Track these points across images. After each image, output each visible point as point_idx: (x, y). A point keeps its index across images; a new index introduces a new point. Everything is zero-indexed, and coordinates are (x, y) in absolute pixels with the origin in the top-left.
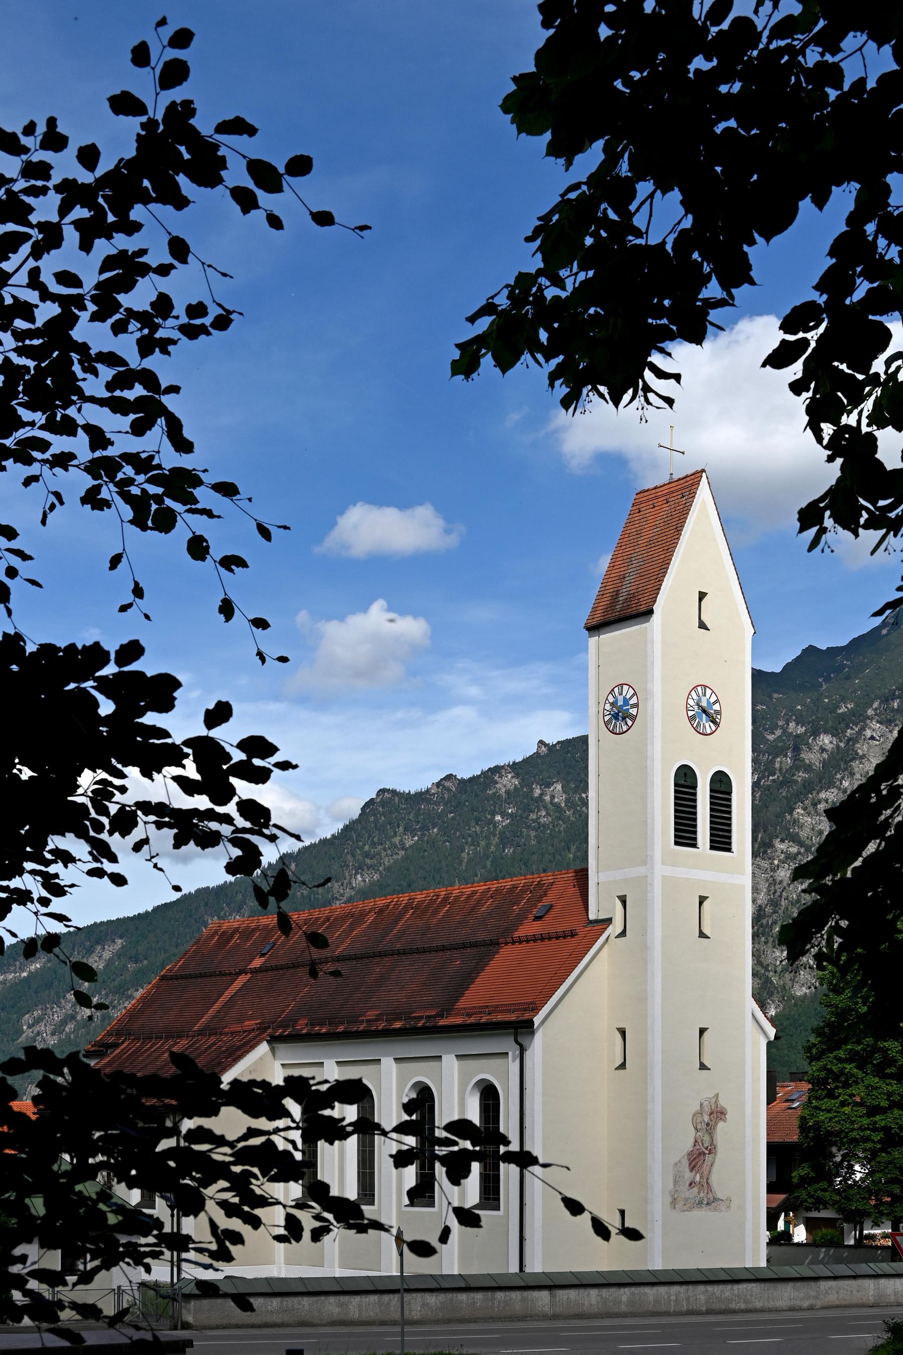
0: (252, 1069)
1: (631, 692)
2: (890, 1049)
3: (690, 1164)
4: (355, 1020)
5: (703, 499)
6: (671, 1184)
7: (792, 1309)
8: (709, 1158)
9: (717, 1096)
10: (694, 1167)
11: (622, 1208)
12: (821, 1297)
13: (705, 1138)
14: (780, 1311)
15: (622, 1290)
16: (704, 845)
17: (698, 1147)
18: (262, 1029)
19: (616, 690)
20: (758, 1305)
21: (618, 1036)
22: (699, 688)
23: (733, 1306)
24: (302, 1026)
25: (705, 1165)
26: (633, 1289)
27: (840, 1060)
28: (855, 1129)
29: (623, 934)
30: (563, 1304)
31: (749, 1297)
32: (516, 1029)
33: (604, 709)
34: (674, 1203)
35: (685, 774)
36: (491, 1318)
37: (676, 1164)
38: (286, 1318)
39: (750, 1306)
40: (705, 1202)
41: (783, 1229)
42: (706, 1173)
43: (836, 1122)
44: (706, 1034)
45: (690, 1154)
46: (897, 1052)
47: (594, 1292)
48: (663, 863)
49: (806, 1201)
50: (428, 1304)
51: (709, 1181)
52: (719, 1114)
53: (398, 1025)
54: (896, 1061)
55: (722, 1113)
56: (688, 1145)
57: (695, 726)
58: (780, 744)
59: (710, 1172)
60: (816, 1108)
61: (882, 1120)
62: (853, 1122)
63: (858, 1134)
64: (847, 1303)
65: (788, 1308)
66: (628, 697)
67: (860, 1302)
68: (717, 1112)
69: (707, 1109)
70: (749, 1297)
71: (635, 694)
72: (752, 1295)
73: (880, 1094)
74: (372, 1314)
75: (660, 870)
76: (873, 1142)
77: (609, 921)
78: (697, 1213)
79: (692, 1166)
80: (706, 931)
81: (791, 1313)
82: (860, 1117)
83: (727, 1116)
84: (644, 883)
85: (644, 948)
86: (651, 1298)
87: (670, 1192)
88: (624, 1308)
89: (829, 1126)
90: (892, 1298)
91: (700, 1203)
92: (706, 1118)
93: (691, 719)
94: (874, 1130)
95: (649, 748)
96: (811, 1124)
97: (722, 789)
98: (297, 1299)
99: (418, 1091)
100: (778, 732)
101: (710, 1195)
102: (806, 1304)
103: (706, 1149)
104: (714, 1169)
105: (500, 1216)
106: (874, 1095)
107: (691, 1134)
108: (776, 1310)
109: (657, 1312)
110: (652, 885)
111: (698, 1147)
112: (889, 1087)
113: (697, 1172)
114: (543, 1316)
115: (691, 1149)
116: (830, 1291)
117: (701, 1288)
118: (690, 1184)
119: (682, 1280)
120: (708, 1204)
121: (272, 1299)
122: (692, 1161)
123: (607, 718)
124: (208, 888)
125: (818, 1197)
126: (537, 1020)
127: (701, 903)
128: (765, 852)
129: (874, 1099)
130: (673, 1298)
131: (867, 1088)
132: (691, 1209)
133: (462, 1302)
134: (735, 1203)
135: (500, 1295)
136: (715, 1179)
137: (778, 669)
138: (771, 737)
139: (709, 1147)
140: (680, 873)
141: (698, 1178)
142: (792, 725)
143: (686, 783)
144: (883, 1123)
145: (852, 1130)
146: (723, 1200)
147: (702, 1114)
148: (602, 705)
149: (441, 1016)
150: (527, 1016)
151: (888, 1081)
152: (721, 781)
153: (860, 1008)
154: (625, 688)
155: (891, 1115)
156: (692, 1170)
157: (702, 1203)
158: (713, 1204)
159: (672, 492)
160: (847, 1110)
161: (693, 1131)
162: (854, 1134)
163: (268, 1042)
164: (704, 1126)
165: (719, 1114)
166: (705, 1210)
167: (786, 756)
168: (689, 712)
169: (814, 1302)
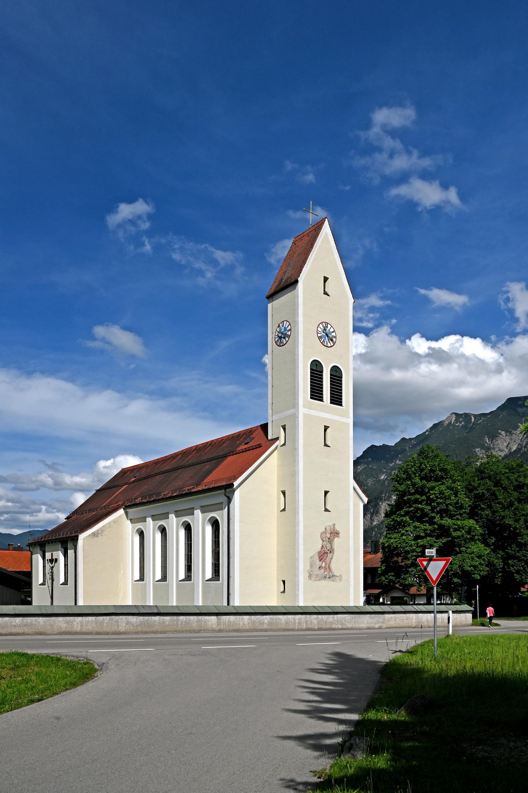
1: (288, 324)
2: (426, 509)
3: (319, 558)
4: (159, 494)
5: (326, 232)
6: (309, 567)
8: (330, 555)
9: (334, 525)
10: (321, 559)
11: (283, 579)
12: (386, 622)
13: (327, 545)
14: (361, 629)
15: (265, 617)
16: (327, 400)
17: (323, 549)
18: (122, 505)
19: (281, 325)
20: (349, 626)
21: (282, 496)
22: (324, 323)
23: (334, 626)
24: (138, 500)
25: (328, 558)
26: (272, 616)
27: (402, 516)
28: (408, 546)
29: (284, 444)
30: (225, 624)
31: (343, 621)
32: (225, 489)
33: (275, 335)
34: (310, 576)
35: (316, 365)
36: (176, 631)
37: (311, 557)
38: (26, 630)
39: (344, 627)
40: (328, 577)
41: (382, 601)
42: (328, 563)
43: (398, 543)
44: (328, 494)
45: (319, 553)
46: (429, 510)
47: (246, 617)
48: (304, 407)
49: (384, 581)
50: (131, 622)
51: (330, 566)
52: (335, 534)
53: (175, 494)
54: (429, 514)
55: (337, 533)
56: (319, 548)
57: (322, 341)
58: (394, 467)
59: (330, 562)
60: (390, 538)
61: (421, 542)
62: (407, 543)
63: (409, 548)
64: (401, 625)
66: (286, 327)
67: (407, 625)
68: (334, 533)
69: (329, 531)
70: (343, 621)
71: (290, 324)
72: (345, 621)
73: (421, 530)
74: (90, 628)
75: (302, 411)
76: (417, 552)
77: (277, 439)
78: (323, 582)
79: (320, 558)
80: (328, 443)
82: (411, 541)
83: (340, 535)
84: (294, 417)
85: (295, 449)
86: (283, 621)
88: (265, 626)
89: (395, 545)
90: (426, 624)
91: (325, 577)
92: (328, 536)
93: (320, 338)
94: (418, 547)
95: (296, 349)
96: (386, 545)
97: (337, 375)
98: (35, 618)
99: (185, 527)
100: (393, 464)
101: (330, 574)
102: (377, 626)
103: (328, 550)
104: (333, 561)
105: (220, 583)
106: (417, 530)
108: (360, 629)
109: (287, 629)
110: (298, 417)
111: (323, 549)
112: (425, 527)
114: (212, 631)
115: (320, 550)
117: (314, 616)
118: (320, 568)
119: (302, 611)
120: (329, 578)
121: (15, 618)
122: (321, 556)
123: (276, 340)
125: (390, 579)
126: (236, 484)
127: (325, 430)
128: (389, 499)
129: (418, 532)
130: (297, 621)
131: (414, 527)
132: (319, 580)
133: (155, 621)
135: (182, 618)
136: (333, 566)
137: (393, 445)
138: (391, 465)
140: (313, 413)
141: (324, 565)
142: (398, 461)
143: (316, 369)
144: (422, 543)
145: (406, 547)
146: (337, 576)
147: (326, 533)
148: (274, 334)
149: (194, 488)
150: (230, 482)
151: (424, 524)
152: (336, 371)
153: (411, 490)
154: (285, 322)
155: (426, 540)
156: (320, 561)
157: (326, 577)
159: (311, 231)
160: (404, 537)
161: (321, 542)
163: (123, 508)
165: (335, 534)
167: (396, 470)
169: (382, 625)
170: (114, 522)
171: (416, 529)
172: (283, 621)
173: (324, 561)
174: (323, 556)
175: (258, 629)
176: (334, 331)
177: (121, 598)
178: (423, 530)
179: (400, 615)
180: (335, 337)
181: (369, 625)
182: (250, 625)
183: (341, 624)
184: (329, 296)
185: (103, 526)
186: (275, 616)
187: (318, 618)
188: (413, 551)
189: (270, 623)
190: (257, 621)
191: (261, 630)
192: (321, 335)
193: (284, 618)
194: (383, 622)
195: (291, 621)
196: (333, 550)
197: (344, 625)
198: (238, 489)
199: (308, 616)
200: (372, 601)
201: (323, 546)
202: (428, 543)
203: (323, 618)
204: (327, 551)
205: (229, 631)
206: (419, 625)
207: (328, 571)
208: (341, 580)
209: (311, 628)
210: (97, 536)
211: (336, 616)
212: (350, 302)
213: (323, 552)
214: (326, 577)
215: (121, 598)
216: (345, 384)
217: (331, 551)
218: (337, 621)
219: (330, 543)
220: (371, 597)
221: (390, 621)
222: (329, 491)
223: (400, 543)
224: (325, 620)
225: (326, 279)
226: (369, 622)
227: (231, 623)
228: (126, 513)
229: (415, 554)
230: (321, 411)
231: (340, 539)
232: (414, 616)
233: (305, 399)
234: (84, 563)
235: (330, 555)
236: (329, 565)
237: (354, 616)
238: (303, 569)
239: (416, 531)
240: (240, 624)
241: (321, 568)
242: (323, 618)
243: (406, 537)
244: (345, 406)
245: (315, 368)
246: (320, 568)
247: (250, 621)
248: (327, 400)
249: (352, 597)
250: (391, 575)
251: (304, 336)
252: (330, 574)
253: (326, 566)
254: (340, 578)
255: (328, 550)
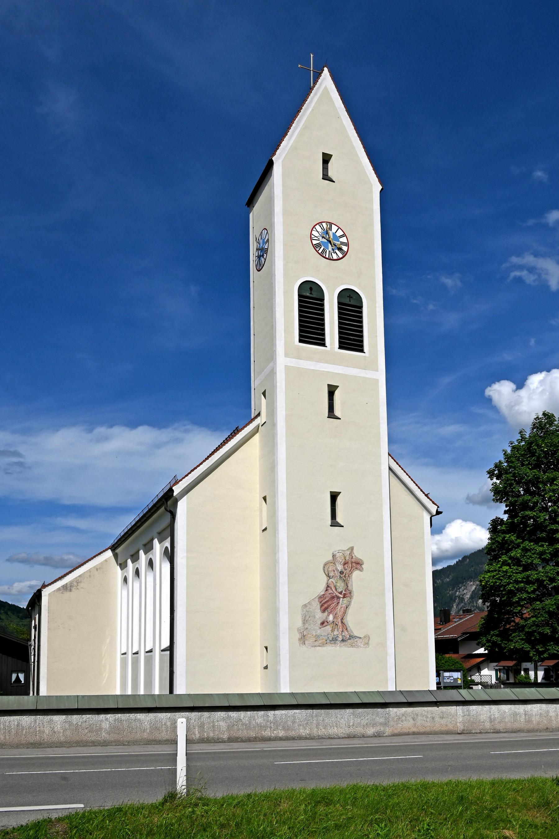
0: (98, 568)
3: (322, 606)
7: (350, 737)
8: (343, 602)
9: (352, 549)
10: (326, 609)
12: (392, 723)
13: (338, 584)
14: (331, 738)
15: (102, 717)
16: (332, 344)
17: (330, 591)
20: (303, 732)
23: (267, 733)
25: (339, 607)
26: (119, 716)
28: (511, 583)
30: (9, 732)
34: (303, 639)
37: (305, 606)
39: (292, 734)
40: (340, 639)
42: (340, 614)
43: (497, 579)
45: (321, 597)
47: (58, 719)
48: (286, 355)
51: (344, 621)
56: (320, 589)
59: (345, 613)
63: (513, 586)
64: (428, 729)
65: (505, 731)
67: (444, 729)
68: (352, 563)
69: (340, 559)
72: (294, 722)
73: (533, 554)
76: (528, 592)
77: (259, 415)
78: (330, 649)
79: (323, 607)
81: (347, 741)
83: (363, 566)
86: (146, 725)
87: (298, 630)
88: (104, 736)
90: (488, 725)
92: (340, 568)
93: (316, 247)
95: (273, 267)
97: (352, 303)
101: (346, 633)
102: (371, 731)
103: (341, 593)
104: (350, 611)
106: (528, 555)
107: (323, 581)
111: (330, 591)
113: (331, 612)
115: (323, 593)
116: (404, 718)
118: (322, 623)
120: (343, 640)
122: (325, 603)
124: (437, 570)
125: (493, 641)
131: (522, 550)
132: (323, 645)
134: (373, 641)
136: (350, 619)
139: (344, 592)
141: (331, 618)
143: (311, 296)
145: (509, 584)
146: (360, 638)
152: (350, 297)
156: (324, 611)
157: (337, 640)
158: (349, 641)
161: (325, 579)
162: (510, 587)
164: (338, 574)
165: (354, 564)
166: (340, 646)
168: (313, 241)
169: (382, 729)
170: (97, 569)
171: (526, 552)
172: (146, 725)
173: (331, 612)
174: (329, 603)
175: (87, 742)
176: (344, 235)
177: (105, 680)
178: (537, 554)
179: (426, 708)
180: (347, 244)
181: (351, 730)
182: (68, 733)
183: (284, 728)
184: (334, 182)
185: (79, 576)
186: (127, 715)
187: (229, 717)
188: (521, 590)
189: (114, 729)
190: (84, 725)
191: (94, 744)
192: (318, 242)
193: (148, 719)
194: (385, 724)
195: (165, 724)
196: (350, 593)
197: (292, 730)
198: (185, 497)
199: (206, 714)
200: (553, 678)
201: (328, 586)
202: (547, 577)
203: (242, 717)
204: (337, 594)
205: (18, 746)
206: (470, 728)
207: (341, 630)
208: (368, 644)
209: (213, 738)
210: (71, 590)
211: (271, 713)
212: (374, 190)
213: (330, 596)
214: (337, 640)
215: (105, 680)
216: (368, 316)
217: (347, 594)
218: (275, 722)
219: (344, 581)
220: (551, 672)
221: (402, 721)
222: (340, 493)
223: (499, 579)
224: (246, 721)
225: (326, 159)
226: (351, 724)
227: (23, 730)
228: (116, 556)
229: (525, 596)
230: (319, 361)
231: (364, 572)
232: (459, 710)
233: (287, 345)
234: (49, 629)
235: (345, 602)
236: (342, 619)
237: (315, 712)
238: (287, 626)
239: (526, 556)
240: (44, 732)
241: (326, 623)
242: (242, 717)
243: (508, 568)
244: (370, 352)
245: (308, 294)
246: (324, 625)
247: (67, 726)
248: (332, 344)
249: (391, 674)
250: (494, 635)
251: (285, 245)
252: (346, 633)
253: (335, 620)
254: (366, 641)
255: (341, 593)
